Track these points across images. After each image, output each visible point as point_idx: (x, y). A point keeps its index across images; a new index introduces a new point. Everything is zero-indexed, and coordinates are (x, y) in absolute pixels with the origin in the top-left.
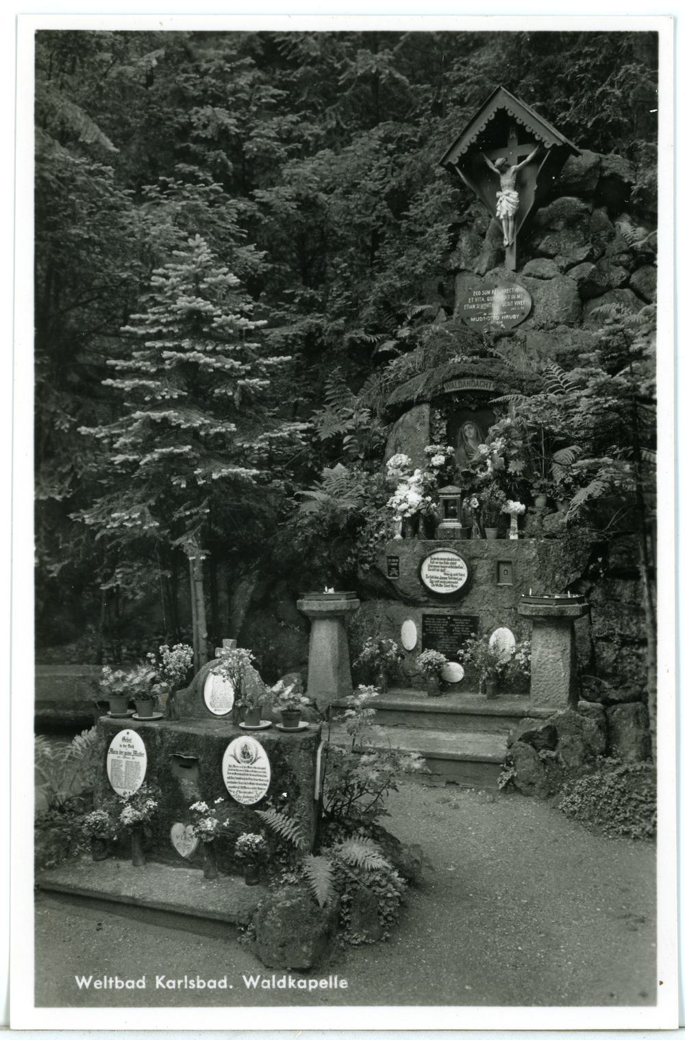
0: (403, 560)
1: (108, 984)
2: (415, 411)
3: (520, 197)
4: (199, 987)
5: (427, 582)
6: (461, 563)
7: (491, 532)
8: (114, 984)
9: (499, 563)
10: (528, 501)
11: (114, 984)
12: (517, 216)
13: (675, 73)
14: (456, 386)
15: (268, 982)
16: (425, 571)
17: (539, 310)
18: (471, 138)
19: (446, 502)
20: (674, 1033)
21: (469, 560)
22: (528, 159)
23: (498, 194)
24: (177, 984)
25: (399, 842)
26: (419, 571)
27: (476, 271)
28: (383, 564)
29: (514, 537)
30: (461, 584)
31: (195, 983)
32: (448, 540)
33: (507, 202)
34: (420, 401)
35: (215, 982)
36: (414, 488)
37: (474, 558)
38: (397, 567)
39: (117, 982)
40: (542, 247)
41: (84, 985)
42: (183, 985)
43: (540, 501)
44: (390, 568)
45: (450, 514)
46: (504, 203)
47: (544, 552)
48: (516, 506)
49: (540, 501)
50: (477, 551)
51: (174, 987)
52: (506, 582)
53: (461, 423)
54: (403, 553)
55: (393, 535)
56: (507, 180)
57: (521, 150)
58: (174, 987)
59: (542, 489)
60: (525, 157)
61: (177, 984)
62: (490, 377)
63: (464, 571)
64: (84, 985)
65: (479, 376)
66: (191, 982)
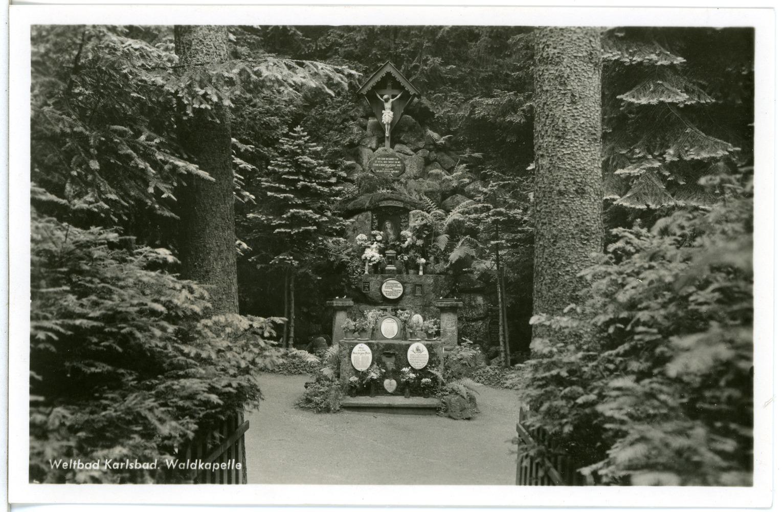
0: (372, 284)
1: (72, 465)
2: (364, 214)
3: (394, 115)
4: (136, 467)
5: (384, 294)
6: (400, 285)
7: (411, 271)
8: (77, 465)
9: (416, 285)
10: (427, 258)
11: (77, 465)
12: (392, 124)
13: (309, 5)
14: (384, 204)
15: (184, 464)
16: (384, 289)
17: (408, 169)
18: (372, 83)
19: (389, 258)
20: (4, 498)
21: (403, 283)
22: (398, 97)
23: (383, 111)
24: (120, 466)
25: (308, 404)
26: (380, 289)
27: (369, 146)
28: (361, 285)
29: (421, 273)
30: (399, 295)
31: (134, 466)
32: (392, 275)
33: (387, 116)
34: (368, 209)
35: (218, 464)
36: (374, 250)
37: (406, 283)
38: (369, 287)
39: (79, 464)
40: (402, 139)
41: (172, 466)
42: (124, 466)
43: (432, 258)
44: (364, 287)
45: (390, 263)
46: (387, 116)
47: (436, 281)
48: (423, 260)
49: (432, 258)
50: (407, 280)
51: (118, 467)
52: (418, 294)
53: (384, 221)
54: (372, 280)
55: (364, 272)
56: (388, 105)
57: (395, 92)
58: (118, 467)
59: (433, 253)
60: (396, 96)
61: (120, 466)
62: (402, 201)
63: (401, 289)
64: (172, 466)
65: (396, 200)
66: (131, 464)
